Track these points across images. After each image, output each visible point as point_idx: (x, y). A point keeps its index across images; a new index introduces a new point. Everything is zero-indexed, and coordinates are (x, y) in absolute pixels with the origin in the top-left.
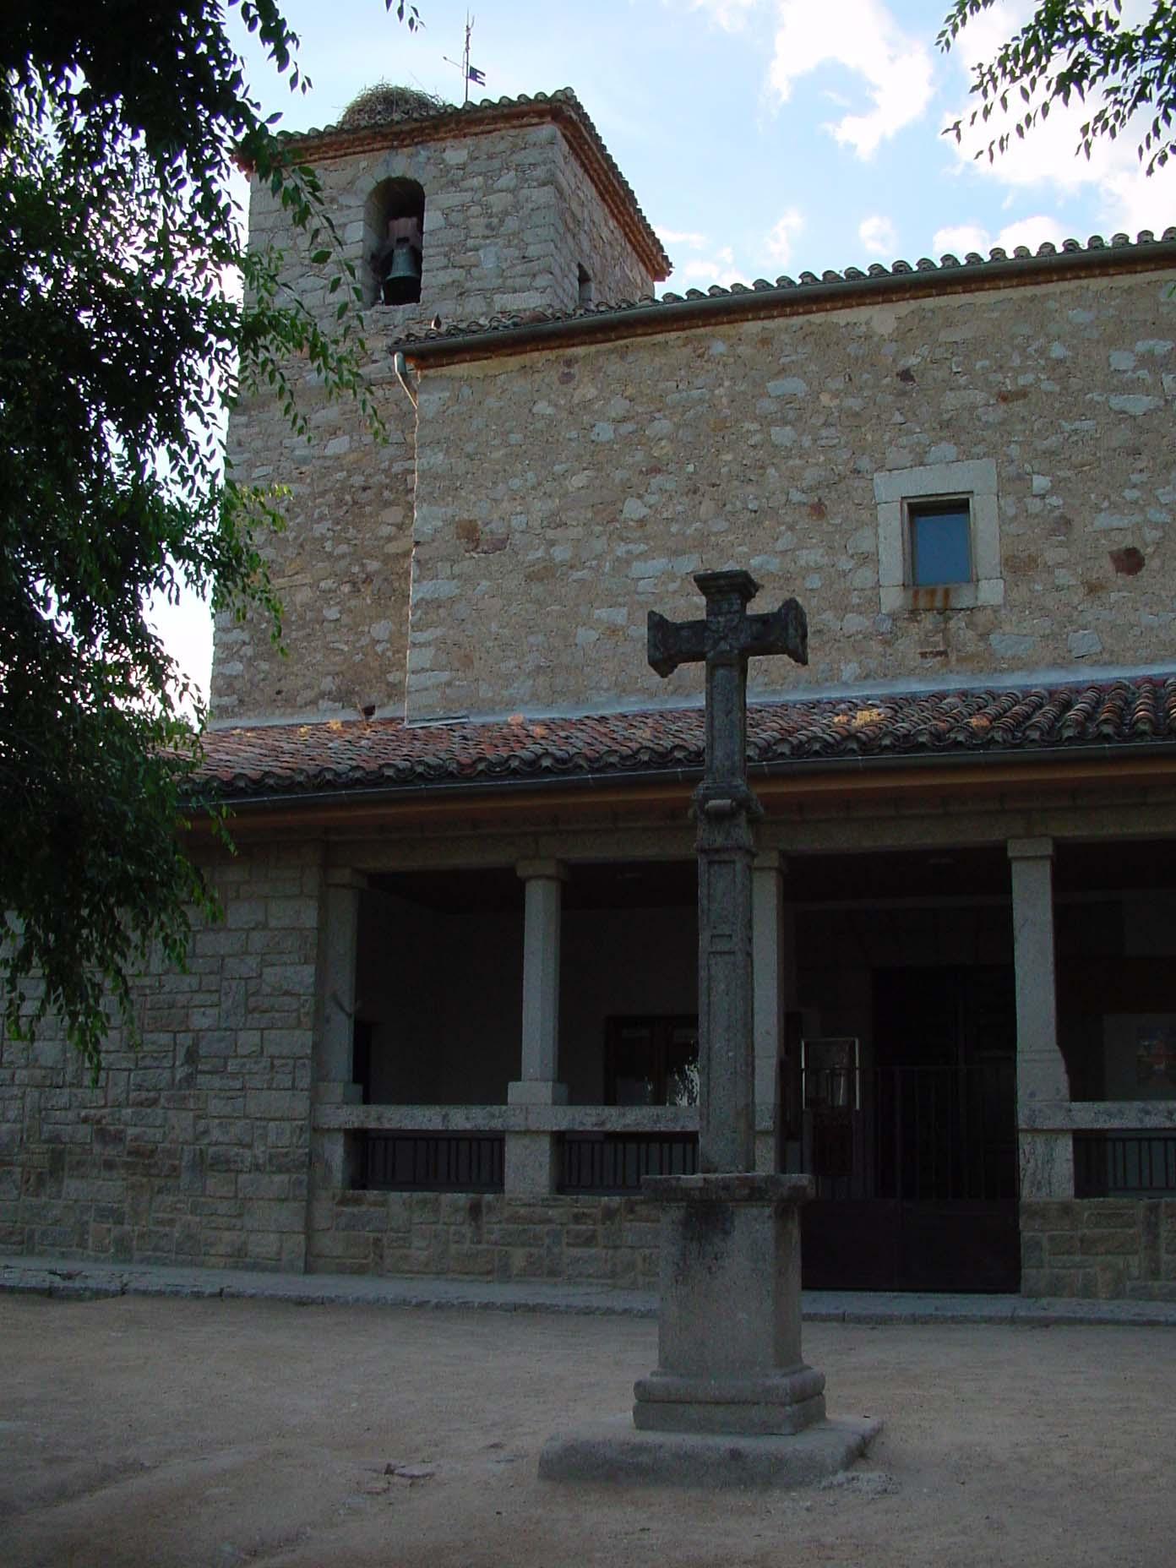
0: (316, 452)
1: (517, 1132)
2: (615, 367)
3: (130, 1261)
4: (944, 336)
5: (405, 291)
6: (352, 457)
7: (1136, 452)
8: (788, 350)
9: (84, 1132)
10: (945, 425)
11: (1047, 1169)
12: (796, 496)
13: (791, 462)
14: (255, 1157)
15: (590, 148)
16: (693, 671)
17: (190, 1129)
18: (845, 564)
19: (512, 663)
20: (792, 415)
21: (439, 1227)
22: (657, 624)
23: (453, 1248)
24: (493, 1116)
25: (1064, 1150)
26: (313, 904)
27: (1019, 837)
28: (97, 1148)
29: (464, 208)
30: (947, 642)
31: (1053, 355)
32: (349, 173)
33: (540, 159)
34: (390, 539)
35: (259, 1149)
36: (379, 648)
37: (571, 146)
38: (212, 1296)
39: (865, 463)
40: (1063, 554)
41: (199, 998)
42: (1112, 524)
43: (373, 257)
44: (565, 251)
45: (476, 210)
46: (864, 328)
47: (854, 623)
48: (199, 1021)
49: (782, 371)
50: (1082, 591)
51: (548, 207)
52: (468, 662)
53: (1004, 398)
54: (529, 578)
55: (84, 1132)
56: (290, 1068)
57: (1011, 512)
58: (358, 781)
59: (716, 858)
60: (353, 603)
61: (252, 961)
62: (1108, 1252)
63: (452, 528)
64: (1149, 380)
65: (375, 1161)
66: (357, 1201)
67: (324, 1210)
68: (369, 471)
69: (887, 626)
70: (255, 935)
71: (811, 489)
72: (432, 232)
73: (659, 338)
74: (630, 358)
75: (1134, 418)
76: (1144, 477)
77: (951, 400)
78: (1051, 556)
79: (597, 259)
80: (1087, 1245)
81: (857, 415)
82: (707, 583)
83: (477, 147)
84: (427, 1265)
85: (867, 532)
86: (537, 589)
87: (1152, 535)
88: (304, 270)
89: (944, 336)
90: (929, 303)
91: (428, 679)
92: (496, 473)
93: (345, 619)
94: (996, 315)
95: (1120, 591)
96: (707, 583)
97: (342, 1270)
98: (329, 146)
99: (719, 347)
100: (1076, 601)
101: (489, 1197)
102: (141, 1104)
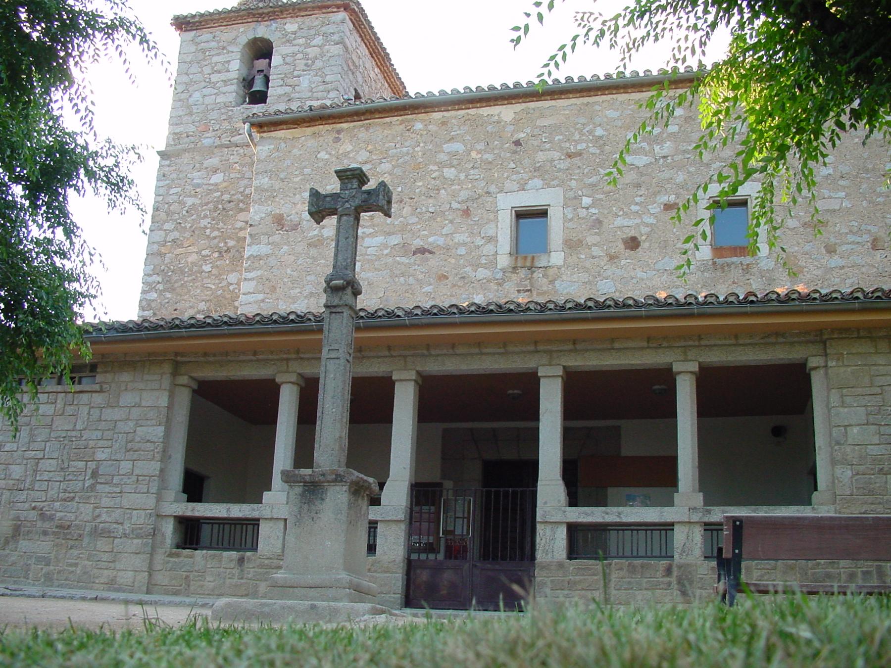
0: (205, 182)
1: (266, 519)
2: (363, 134)
3: (52, 586)
4: (539, 123)
5: (259, 98)
6: (225, 184)
7: (638, 186)
8: (456, 128)
9: (33, 515)
10: (537, 169)
11: (551, 543)
12: (455, 205)
13: (453, 187)
14: (124, 529)
15: (365, 28)
16: (331, 222)
17: (91, 514)
18: (479, 242)
19: (298, 290)
20: (455, 162)
21: (222, 570)
22: (315, 195)
23: (228, 581)
24: (254, 510)
25: (562, 533)
26: (167, 393)
27: (544, 365)
28: (39, 524)
29: (294, 54)
30: (532, 284)
31: (597, 134)
32: (233, 35)
33: (336, 30)
34: (241, 229)
35: (127, 526)
36: (231, 288)
37: (354, 25)
38: (91, 599)
39: (493, 189)
40: (598, 238)
41: (101, 444)
42: (623, 224)
43: (244, 80)
44: (347, 80)
45: (300, 56)
46: (496, 118)
47: (482, 273)
48: (100, 455)
49: (452, 139)
50: (606, 259)
51: (339, 56)
52: (273, 289)
53: (569, 156)
54: (310, 245)
55: (33, 515)
56: (147, 482)
57: (570, 216)
58: (192, 326)
59: (334, 310)
60: (219, 263)
61: (131, 424)
62: (583, 589)
63: (270, 217)
64: (647, 148)
65: (191, 533)
66: (178, 555)
67: (159, 558)
68: (233, 192)
69: (500, 275)
70: (134, 410)
71: (463, 202)
72: (275, 67)
73: (388, 120)
74: (371, 131)
75: (639, 168)
76: (642, 199)
77: (541, 156)
78: (591, 240)
79: (366, 88)
80: (571, 585)
81: (490, 163)
82: (342, 175)
83: (303, 23)
84: (213, 590)
85: (493, 225)
86: (313, 252)
87: (645, 230)
88: (206, 84)
89: (539, 123)
90: (532, 105)
91: (251, 298)
92: (296, 189)
93: (215, 272)
94: (567, 112)
95: (627, 259)
96: (342, 175)
97: (167, 593)
98: (224, 19)
99: (419, 126)
100: (603, 264)
101: (248, 554)
102: (65, 500)
